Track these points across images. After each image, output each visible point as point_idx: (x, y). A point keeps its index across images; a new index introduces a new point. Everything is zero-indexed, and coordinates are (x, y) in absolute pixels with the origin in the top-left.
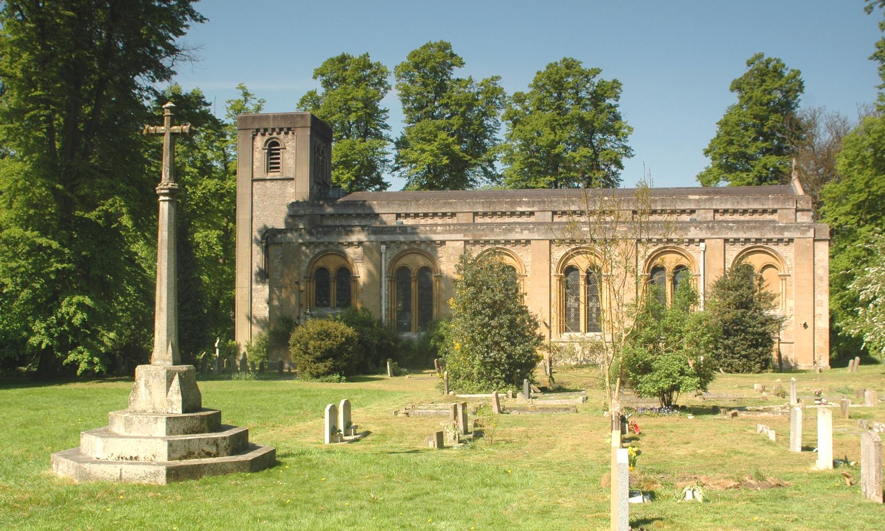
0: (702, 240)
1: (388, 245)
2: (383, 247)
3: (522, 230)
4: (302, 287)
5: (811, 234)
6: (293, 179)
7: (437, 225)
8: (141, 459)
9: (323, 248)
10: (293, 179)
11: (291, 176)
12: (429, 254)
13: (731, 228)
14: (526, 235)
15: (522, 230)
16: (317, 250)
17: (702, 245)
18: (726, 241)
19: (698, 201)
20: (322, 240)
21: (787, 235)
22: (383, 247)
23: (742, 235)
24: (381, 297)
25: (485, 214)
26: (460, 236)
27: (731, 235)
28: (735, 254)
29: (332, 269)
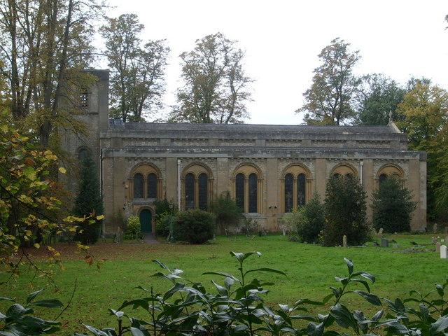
0: (362, 160)
1: (183, 159)
2: (179, 161)
3: (262, 152)
4: (127, 186)
5: (418, 157)
6: (98, 113)
7: (195, 147)
8: (290, 274)
9: (140, 161)
10: (98, 113)
11: (96, 111)
12: (306, 167)
13: (377, 153)
14: (264, 155)
15: (262, 152)
16: (136, 163)
17: (362, 162)
18: (374, 160)
19: (348, 135)
20: (140, 156)
21: (406, 157)
22: (179, 161)
23: (382, 157)
24: (178, 192)
25: (226, 140)
26: (226, 155)
27: (377, 157)
28: (379, 168)
29: (197, 175)
